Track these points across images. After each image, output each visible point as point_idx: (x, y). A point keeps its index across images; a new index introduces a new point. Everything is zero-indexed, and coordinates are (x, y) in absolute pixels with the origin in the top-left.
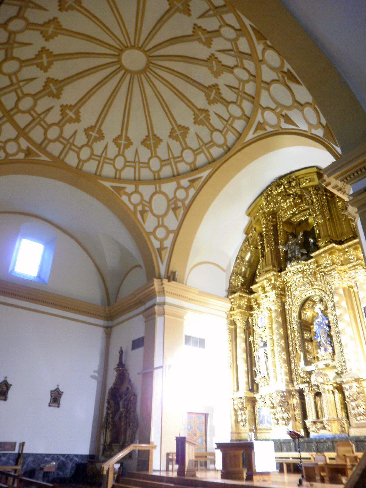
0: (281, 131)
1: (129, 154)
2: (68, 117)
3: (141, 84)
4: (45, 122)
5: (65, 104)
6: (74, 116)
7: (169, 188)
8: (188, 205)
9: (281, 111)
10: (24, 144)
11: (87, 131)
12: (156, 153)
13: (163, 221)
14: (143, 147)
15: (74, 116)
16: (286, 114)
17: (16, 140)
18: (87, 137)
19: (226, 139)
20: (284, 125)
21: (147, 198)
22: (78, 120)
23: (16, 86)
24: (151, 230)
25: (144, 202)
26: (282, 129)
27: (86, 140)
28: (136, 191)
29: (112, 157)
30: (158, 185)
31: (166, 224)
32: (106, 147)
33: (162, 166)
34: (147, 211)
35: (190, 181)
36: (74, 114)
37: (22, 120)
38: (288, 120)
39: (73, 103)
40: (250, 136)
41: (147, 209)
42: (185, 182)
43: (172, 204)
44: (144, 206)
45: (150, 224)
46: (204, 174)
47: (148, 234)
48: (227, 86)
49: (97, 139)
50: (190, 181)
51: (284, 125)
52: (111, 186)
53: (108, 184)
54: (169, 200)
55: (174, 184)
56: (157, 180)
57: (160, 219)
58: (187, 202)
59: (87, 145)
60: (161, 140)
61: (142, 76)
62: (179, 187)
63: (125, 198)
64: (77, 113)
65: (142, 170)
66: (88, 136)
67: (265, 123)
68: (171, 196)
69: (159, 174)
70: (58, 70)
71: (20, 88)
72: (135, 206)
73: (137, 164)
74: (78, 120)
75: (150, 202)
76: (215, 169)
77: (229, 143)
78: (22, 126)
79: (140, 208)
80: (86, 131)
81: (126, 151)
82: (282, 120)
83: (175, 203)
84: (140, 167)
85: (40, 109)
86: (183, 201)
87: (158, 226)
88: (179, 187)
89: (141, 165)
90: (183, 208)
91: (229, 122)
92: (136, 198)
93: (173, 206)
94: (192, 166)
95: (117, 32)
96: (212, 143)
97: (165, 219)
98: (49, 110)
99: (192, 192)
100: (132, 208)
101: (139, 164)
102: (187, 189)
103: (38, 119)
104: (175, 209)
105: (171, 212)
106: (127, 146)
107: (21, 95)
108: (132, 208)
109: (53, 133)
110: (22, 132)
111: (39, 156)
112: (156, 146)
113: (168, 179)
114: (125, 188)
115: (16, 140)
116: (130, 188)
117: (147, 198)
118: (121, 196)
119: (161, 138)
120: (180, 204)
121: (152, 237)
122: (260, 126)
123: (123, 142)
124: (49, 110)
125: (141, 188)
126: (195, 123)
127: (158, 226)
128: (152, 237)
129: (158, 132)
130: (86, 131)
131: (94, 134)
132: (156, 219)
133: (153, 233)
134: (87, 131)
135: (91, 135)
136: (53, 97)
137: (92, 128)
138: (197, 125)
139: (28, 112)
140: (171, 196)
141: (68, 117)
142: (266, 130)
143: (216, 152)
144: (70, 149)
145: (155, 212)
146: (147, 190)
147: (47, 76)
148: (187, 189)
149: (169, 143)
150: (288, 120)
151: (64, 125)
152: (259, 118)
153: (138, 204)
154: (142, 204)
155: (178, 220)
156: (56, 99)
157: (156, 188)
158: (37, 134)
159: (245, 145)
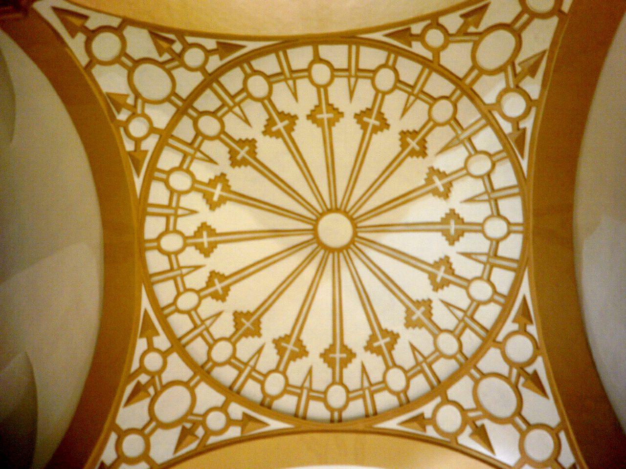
0: (455, 445)
1: (209, 307)
2: (212, 190)
3: (372, 243)
4: (191, 162)
5: (227, 177)
6: (215, 198)
7: (208, 397)
8: (211, 445)
9: (479, 418)
10: (150, 144)
11: (204, 227)
12: (238, 339)
13: (153, 430)
14: (232, 317)
15: (215, 198)
16: (483, 426)
17: (152, 130)
18: (195, 233)
19: (345, 406)
20: (466, 440)
21: (166, 377)
22: (213, 206)
23: (231, 103)
24: (124, 426)
25: (157, 379)
26: (457, 443)
27: (191, 233)
28: (165, 354)
29: (188, 286)
30: (198, 378)
31: (153, 439)
32: (259, 351)
33: (228, 362)
34: (149, 394)
35: (245, 415)
36: (221, 197)
37: (185, 130)
38: (481, 434)
39: (234, 188)
40: (392, 424)
41: (151, 390)
42: (236, 410)
43: (189, 421)
44: (151, 382)
45: (131, 415)
46: (275, 425)
47: (117, 429)
48: (403, 114)
49: (199, 247)
50: (245, 415)
51: (466, 440)
52: (146, 311)
53: (145, 304)
54: (190, 411)
55: (219, 399)
56: (203, 371)
57: (153, 424)
58: (213, 440)
59: (185, 238)
60: (259, 335)
61: (322, 252)
62: (223, 408)
63: (141, 344)
64: (222, 200)
65: (200, 339)
66: (198, 233)
67: (433, 421)
68: (199, 409)
69: (212, 368)
70: (271, 150)
71: (230, 109)
72: (142, 369)
73: (203, 327)
74: (213, 206)
75: (165, 387)
76: (296, 430)
77: (412, 393)
78: (175, 133)
79: (143, 378)
80: (204, 227)
81: (209, 299)
82: (468, 430)
83: (195, 424)
84: (201, 335)
85: (209, 147)
86: (208, 433)
87: (140, 432)
88: (223, 408)
89: (205, 333)
90: (199, 444)
91: (373, 388)
92: (153, 361)
93: (188, 425)
94: (268, 400)
95: (358, 192)
96: (323, 397)
97: (159, 431)
98: (211, 160)
99: (234, 432)
100: (135, 365)
101: (204, 330)
102: (230, 422)
103: (193, 149)
104: (185, 435)
105: (176, 432)
106: (216, 296)
107: (220, 114)
108: (135, 365)
109: (180, 181)
110: (166, 137)
111: (138, 174)
112: (246, 334)
113: (217, 385)
114: (157, 334)
115: (152, 130)
116: (162, 342)
117: (166, 377)
118: (141, 336)
119: (263, 332)
120: (200, 432)
121: (113, 437)
122: (420, 419)
123: (218, 286)
124: (211, 160)
125: (174, 359)
126: (322, 355)
127: (140, 432)
128: (113, 437)
129: (267, 322)
130: (204, 227)
131: (205, 240)
132: (147, 418)
133: (122, 434)
134: (204, 227)
135: (202, 236)
136: (230, 158)
137: (212, 232)
138: (322, 360)
139: (198, 133)
140: (199, 409)
141: (212, 190)
142: (425, 430)
143: (317, 410)
144: (167, 217)
145: (157, 407)
146: (177, 369)
147: (257, 138)
148: (230, 422)
149: (264, 348)
150: (481, 434)
151: (198, 190)
152: (427, 410)
153: (148, 372)
154: (153, 377)
155: (177, 449)
156: (229, 162)
157: (191, 379)
158: (169, 159)
159: (372, 430)
